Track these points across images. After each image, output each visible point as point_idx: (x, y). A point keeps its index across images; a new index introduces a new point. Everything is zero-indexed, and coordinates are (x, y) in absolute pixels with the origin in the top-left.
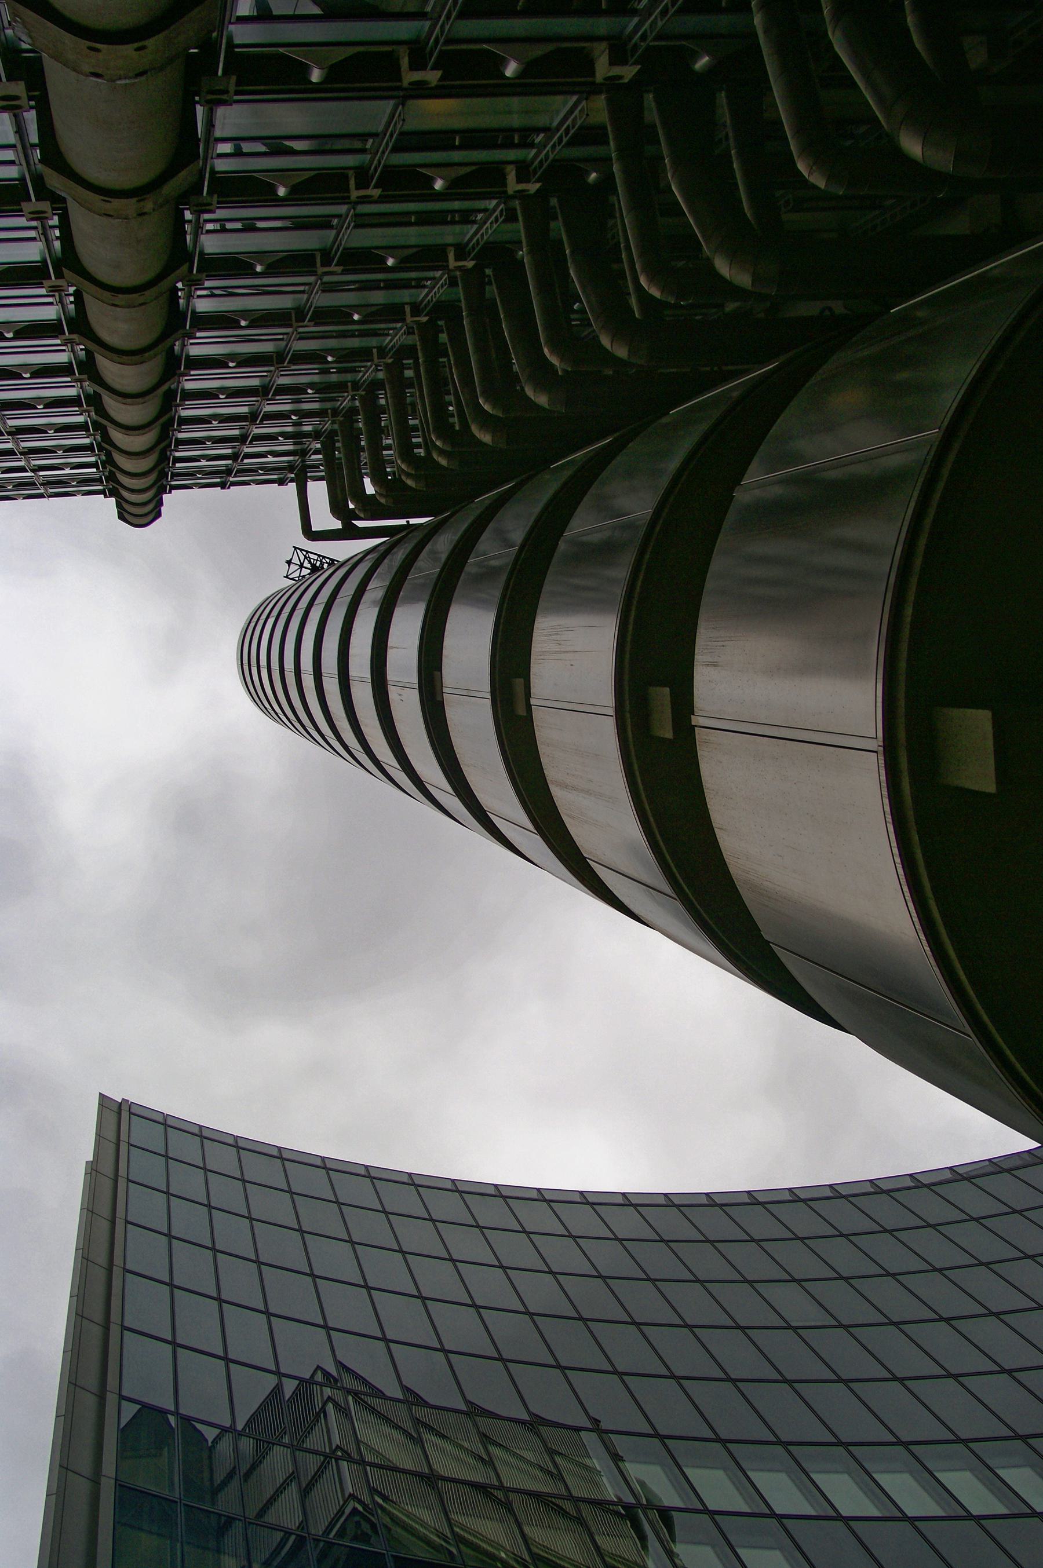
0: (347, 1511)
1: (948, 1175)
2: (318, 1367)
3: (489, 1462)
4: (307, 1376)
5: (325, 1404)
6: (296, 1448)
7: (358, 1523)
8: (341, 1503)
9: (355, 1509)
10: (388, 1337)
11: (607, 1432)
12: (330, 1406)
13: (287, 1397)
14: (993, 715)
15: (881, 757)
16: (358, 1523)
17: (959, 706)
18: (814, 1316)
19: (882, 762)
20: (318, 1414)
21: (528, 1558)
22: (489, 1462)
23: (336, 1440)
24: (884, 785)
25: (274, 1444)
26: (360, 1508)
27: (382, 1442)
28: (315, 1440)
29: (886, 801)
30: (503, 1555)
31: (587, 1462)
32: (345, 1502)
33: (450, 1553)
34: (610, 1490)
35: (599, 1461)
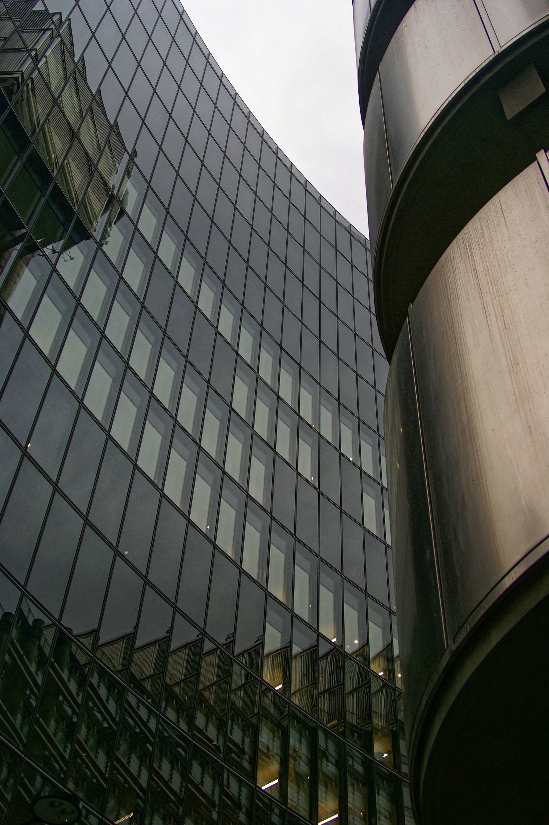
0: (15, 75)
1: (347, 226)
2: (60, 13)
3: (101, 151)
4: (51, 11)
5: (48, 29)
6: (17, 31)
7: (14, 84)
8: (16, 70)
9: (18, 78)
10: (95, 35)
11: (135, 163)
12: (49, 33)
13: (33, 10)
14: (545, 94)
15: (493, 57)
16: (14, 84)
17: (539, 73)
18: (248, 214)
19: (491, 58)
20: (42, 30)
21: (60, 163)
22: (101, 151)
23: (38, 47)
24: (481, 67)
25: (11, 19)
26: (20, 80)
27: (52, 66)
28: (29, 38)
29: (474, 74)
30: (53, 156)
31: (117, 164)
32: (18, 72)
33: (35, 129)
34: (113, 181)
35: (121, 168)
